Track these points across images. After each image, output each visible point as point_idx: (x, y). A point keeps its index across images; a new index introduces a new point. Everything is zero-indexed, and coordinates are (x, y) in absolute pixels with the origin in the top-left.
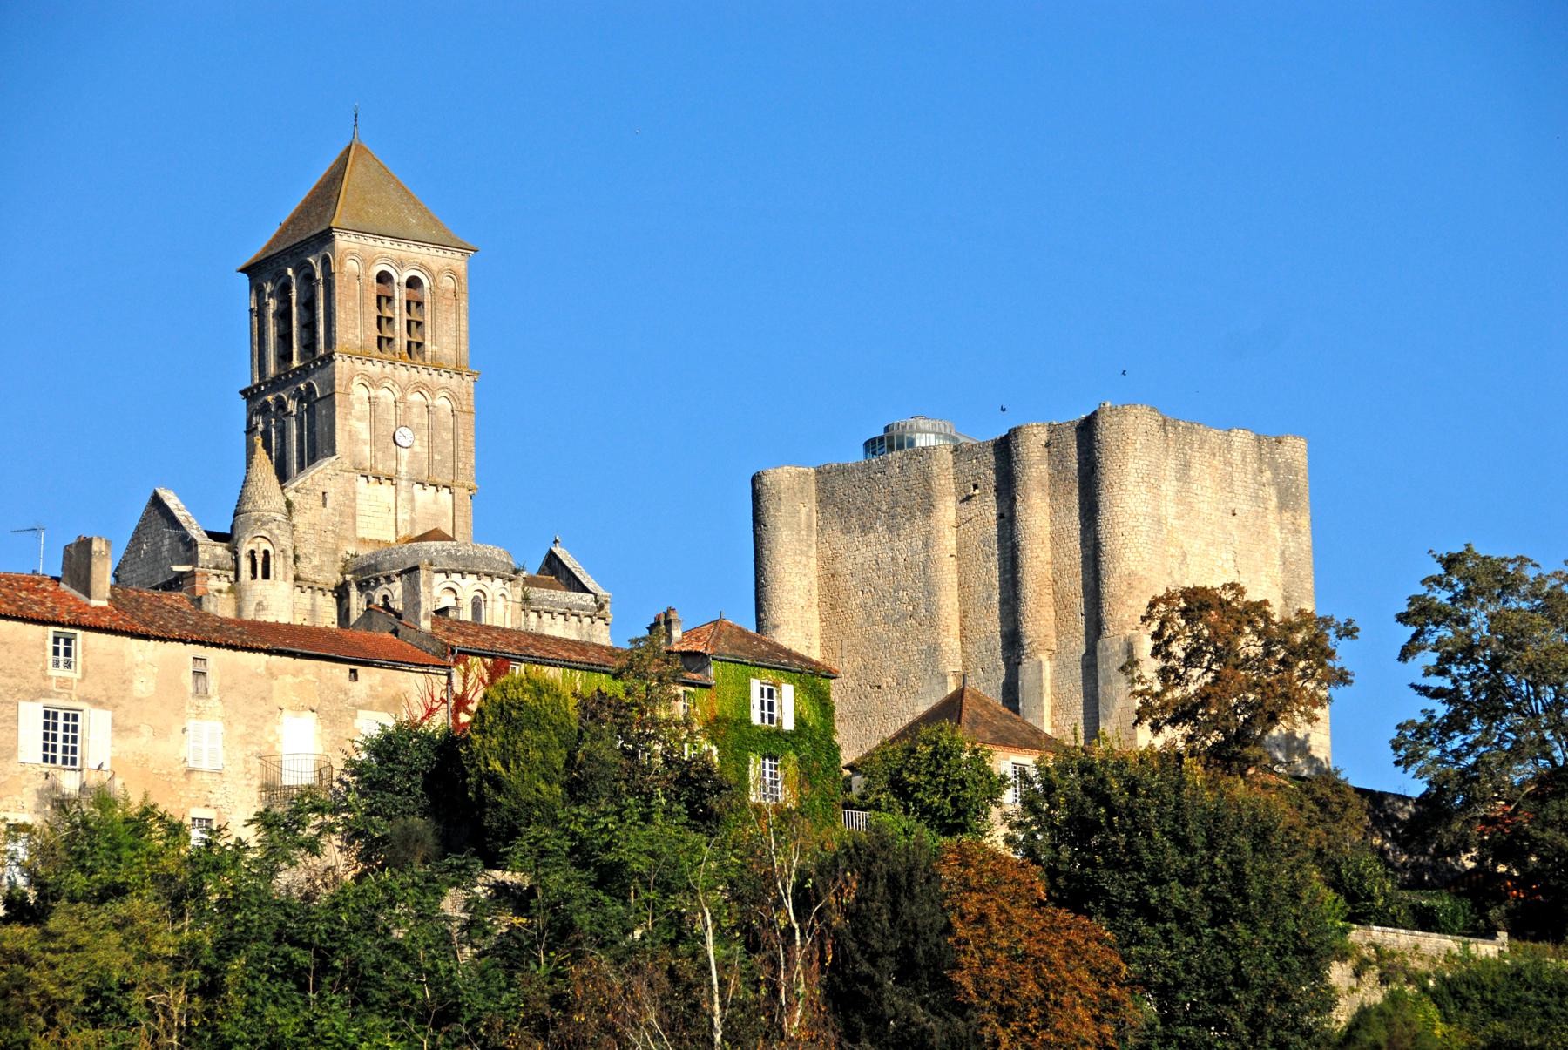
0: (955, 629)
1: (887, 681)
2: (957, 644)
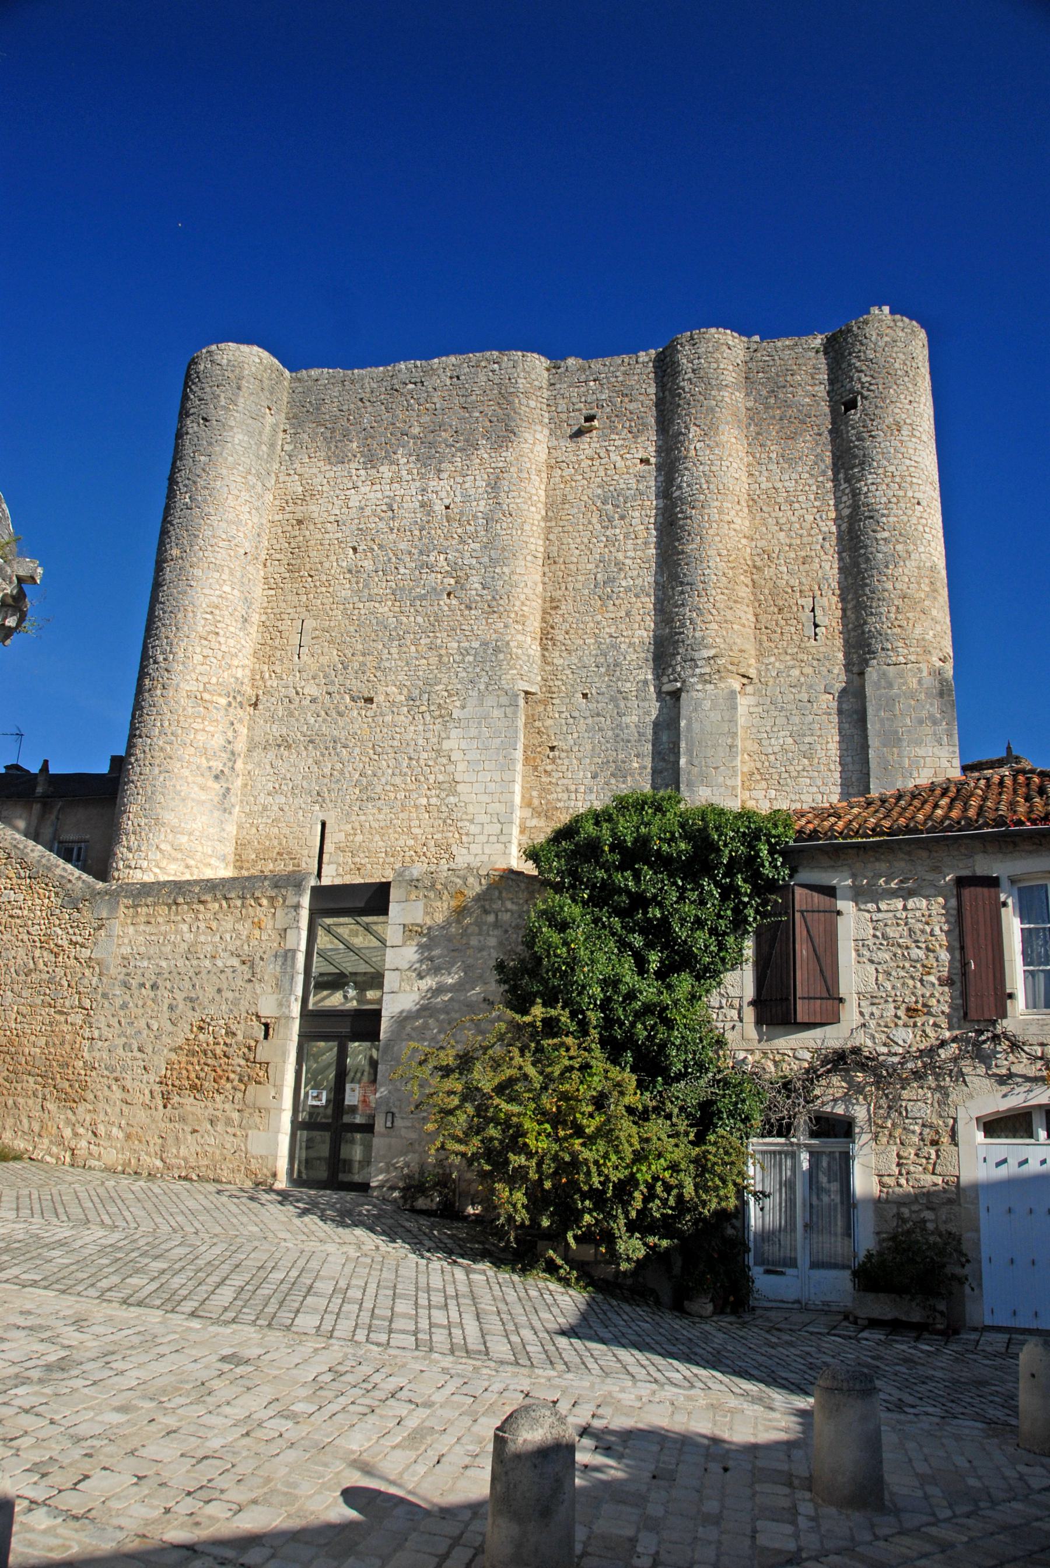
0: (535, 624)
1: (387, 691)
2: (535, 650)
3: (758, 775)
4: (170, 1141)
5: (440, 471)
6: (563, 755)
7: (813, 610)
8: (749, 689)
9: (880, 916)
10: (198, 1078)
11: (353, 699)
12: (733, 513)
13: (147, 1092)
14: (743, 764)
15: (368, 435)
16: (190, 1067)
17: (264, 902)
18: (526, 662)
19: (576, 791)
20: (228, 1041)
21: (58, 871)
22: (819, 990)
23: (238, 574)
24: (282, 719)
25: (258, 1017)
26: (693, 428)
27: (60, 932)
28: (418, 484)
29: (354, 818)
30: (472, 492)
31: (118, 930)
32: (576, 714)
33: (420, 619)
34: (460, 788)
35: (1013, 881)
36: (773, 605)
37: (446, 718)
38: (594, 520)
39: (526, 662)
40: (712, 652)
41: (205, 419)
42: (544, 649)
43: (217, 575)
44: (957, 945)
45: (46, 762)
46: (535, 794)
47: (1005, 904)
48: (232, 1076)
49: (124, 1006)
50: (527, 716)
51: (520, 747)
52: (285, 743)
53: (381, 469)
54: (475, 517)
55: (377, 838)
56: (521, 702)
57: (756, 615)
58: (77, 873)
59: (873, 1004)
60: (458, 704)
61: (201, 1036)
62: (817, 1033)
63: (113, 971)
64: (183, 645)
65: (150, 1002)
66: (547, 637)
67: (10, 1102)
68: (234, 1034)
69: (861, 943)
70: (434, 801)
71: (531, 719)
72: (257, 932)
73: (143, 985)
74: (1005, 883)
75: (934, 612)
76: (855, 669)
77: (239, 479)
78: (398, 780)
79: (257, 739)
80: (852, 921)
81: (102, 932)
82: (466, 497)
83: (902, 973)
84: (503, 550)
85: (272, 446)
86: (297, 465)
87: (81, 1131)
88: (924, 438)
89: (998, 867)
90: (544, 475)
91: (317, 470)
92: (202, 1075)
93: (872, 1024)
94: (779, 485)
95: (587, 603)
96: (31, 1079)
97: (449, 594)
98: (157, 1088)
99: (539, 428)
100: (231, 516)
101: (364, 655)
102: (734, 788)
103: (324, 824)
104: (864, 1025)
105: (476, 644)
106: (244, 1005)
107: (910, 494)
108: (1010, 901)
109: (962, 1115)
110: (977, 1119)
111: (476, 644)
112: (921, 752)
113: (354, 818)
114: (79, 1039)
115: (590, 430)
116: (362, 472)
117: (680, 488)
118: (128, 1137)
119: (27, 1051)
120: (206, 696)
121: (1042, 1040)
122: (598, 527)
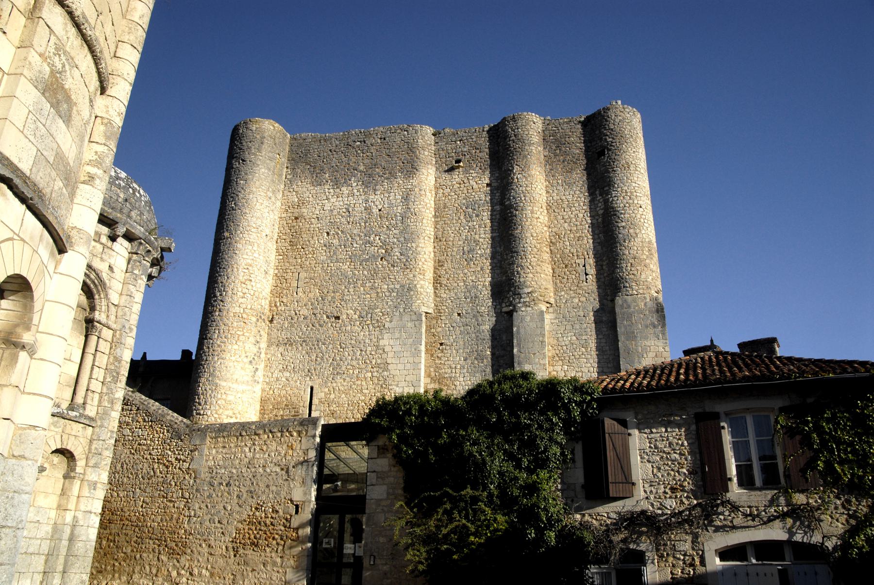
0: (430, 275)
1: (348, 312)
2: (430, 289)
3: (559, 357)
4: (238, 577)
5: (375, 190)
6: (448, 348)
7: (584, 266)
8: (551, 310)
9: (653, 435)
10: (255, 538)
11: (328, 317)
12: (539, 213)
13: (224, 547)
14: (549, 351)
15: (334, 170)
16: (251, 532)
17: (295, 434)
18: (426, 297)
19: (455, 368)
20: (274, 516)
21: (169, 418)
22: (620, 478)
23: (263, 247)
24: (287, 329)
25: (292, 501)
26: (516, 167)
27: (170, 453)
28: (363, 197)
29: (329, 384)
30: (394, 201)
31: (206, 452)
32: (454, 325)
33: (366, 273)
34: (390, 367)
35: (727, 414)
36: (562, 264)
37: (381, 327)
38: (462, 218)
39: (426, 297)
40: (530, 290)
41: (243, 161)
42: (436, 288)
43: (250, 247)
44: (697, 451)
45: (145, 354)
46: (432, 369)
47: (723, 428)
48: (277, 536)
49: (210, 496)
50: (427, 326)
51: (423, 343)
52: (289, 343)
53: (343, 189)
54: (396, 216)
55: (343, 396)
56: (424, 318)
57: (553, 269)
58: (180, 418)
59: (651, 486)
60: (388, 320)
61: (257, 513)
62: (620, 503)
63: (203, 476)
64: (231, 287)
65: (226, 494)
66: (437, 282)
67: (138, 556)
68: (277, 512)
69: (642, 451)
70: (375, 374)
71: (429, 328)
72: (290, 452)
73: (221, 484)
74: (722, 416)
75: (651, 266)
76: (609, 298)
77: (262, 194)
78: (354, 363)
79: (273, 340)
80: (637, 440)
81: (196, 453)
82: (390, 204)
83: (667, 468)
84: (412, 234)
85: (281, 175)
86: (295, 187)
87: (183, 572)
88: (642, 171)
89: (720, 408)
90: (433, 193)
91: (305, 188)
92: (258, 536)
93: (652, 497)
94: (564, 198)
95: (459, 263)
96: (151, 542)
97: (382, 259)
98: (230, 545)
99: (430, 166)
100: (259, 214)
101: (334, 292)
102: (544, 365)
103: (312, 388)
104: (647, 498)
105: (398, 286)
106: (283, 494)
107: (636, 202)
108: (726, 426)
109: (706, 548)
110: (716, 550)
111: (398, 286)
112: (648, 343)
113: (329, 384)
114: (182, 517)
115: (458, 167)
116: (332, 190)
117: (509, 199)
118: (212, 575)
119: (149, 524)
120: (245, 316)
121: (749, 504)
122: (464, 221)
